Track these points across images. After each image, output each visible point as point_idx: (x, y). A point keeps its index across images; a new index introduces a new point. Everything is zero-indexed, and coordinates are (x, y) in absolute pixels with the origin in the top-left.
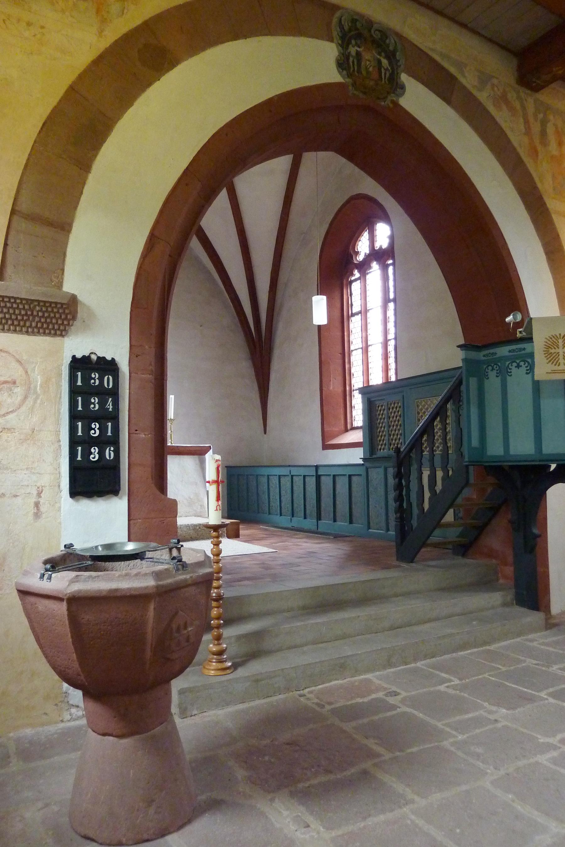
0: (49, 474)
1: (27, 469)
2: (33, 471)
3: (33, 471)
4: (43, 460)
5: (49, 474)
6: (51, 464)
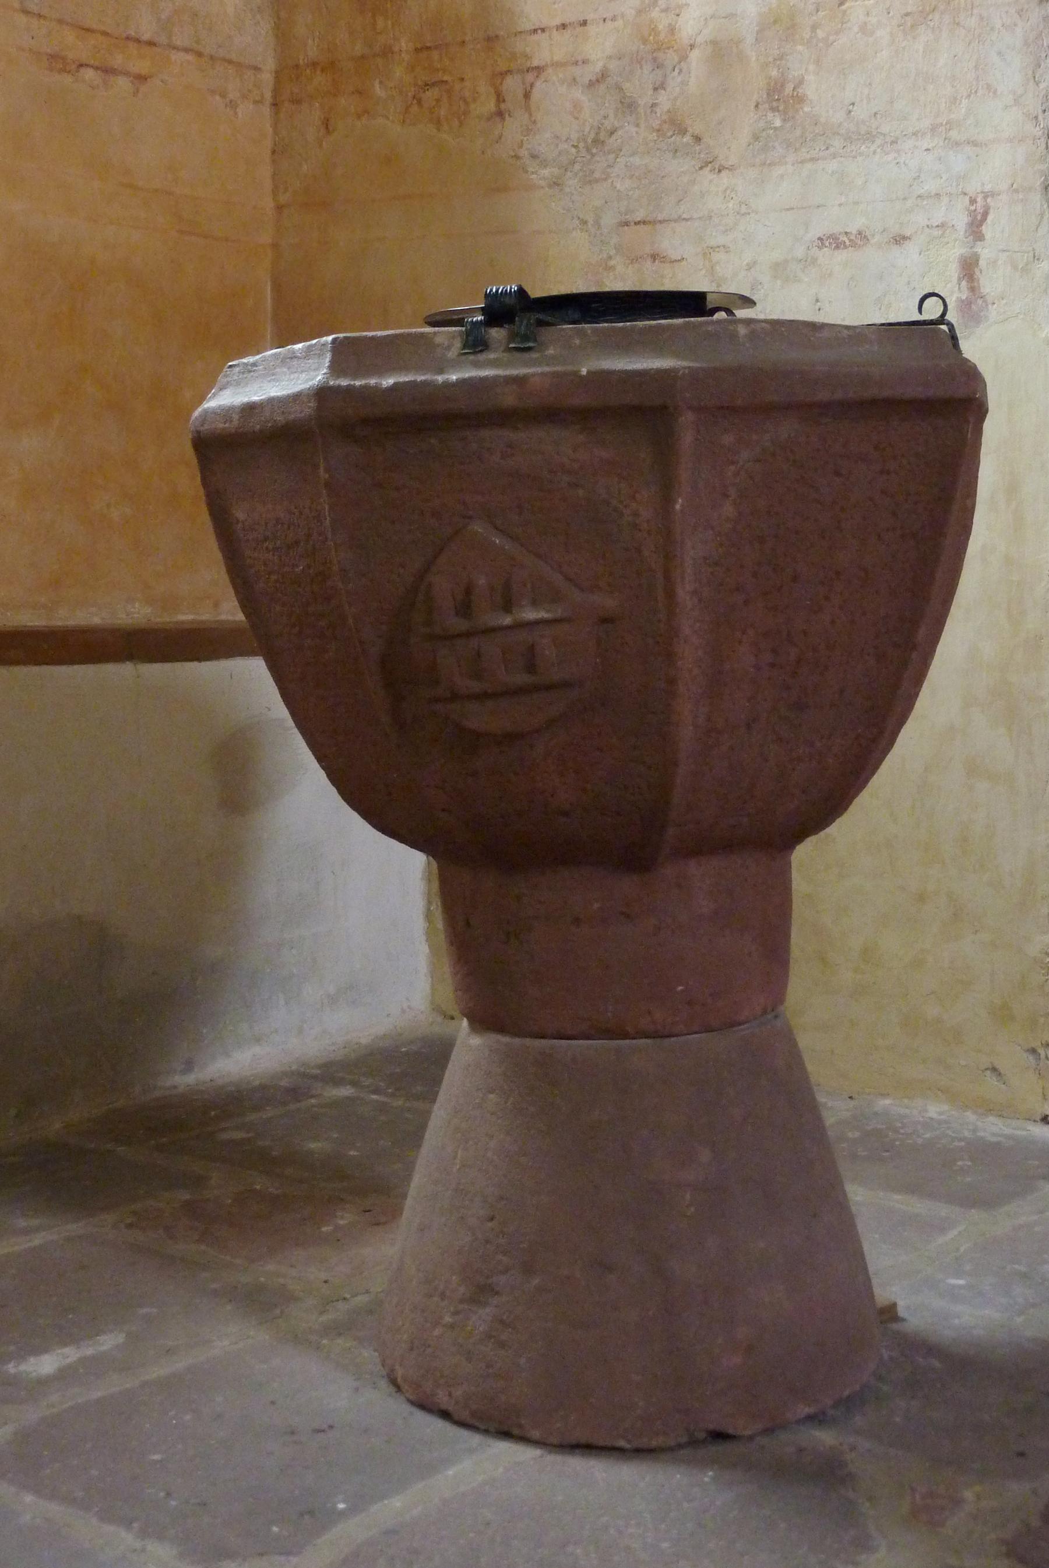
0: (1010, 140)
1: (934, 129)
2: (954, 134)
3: (954, 134)
4: (989, 87)
5: (1010, 140)
6: (1017, 101)
